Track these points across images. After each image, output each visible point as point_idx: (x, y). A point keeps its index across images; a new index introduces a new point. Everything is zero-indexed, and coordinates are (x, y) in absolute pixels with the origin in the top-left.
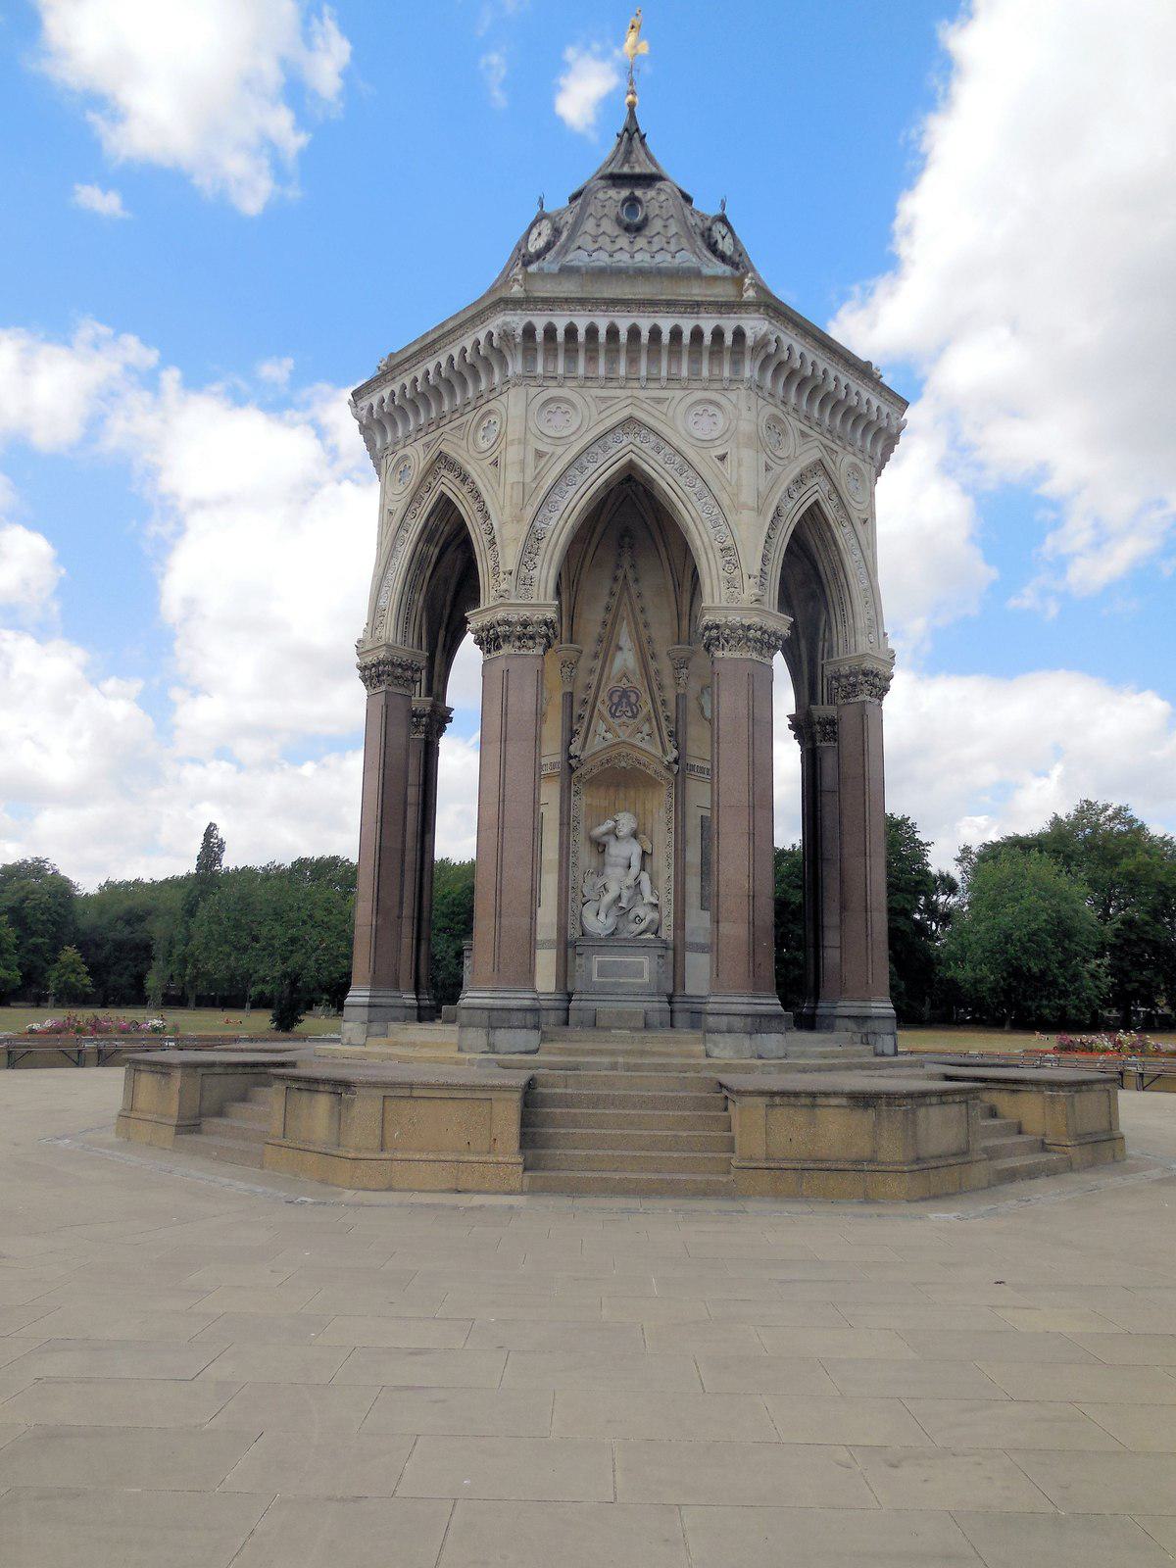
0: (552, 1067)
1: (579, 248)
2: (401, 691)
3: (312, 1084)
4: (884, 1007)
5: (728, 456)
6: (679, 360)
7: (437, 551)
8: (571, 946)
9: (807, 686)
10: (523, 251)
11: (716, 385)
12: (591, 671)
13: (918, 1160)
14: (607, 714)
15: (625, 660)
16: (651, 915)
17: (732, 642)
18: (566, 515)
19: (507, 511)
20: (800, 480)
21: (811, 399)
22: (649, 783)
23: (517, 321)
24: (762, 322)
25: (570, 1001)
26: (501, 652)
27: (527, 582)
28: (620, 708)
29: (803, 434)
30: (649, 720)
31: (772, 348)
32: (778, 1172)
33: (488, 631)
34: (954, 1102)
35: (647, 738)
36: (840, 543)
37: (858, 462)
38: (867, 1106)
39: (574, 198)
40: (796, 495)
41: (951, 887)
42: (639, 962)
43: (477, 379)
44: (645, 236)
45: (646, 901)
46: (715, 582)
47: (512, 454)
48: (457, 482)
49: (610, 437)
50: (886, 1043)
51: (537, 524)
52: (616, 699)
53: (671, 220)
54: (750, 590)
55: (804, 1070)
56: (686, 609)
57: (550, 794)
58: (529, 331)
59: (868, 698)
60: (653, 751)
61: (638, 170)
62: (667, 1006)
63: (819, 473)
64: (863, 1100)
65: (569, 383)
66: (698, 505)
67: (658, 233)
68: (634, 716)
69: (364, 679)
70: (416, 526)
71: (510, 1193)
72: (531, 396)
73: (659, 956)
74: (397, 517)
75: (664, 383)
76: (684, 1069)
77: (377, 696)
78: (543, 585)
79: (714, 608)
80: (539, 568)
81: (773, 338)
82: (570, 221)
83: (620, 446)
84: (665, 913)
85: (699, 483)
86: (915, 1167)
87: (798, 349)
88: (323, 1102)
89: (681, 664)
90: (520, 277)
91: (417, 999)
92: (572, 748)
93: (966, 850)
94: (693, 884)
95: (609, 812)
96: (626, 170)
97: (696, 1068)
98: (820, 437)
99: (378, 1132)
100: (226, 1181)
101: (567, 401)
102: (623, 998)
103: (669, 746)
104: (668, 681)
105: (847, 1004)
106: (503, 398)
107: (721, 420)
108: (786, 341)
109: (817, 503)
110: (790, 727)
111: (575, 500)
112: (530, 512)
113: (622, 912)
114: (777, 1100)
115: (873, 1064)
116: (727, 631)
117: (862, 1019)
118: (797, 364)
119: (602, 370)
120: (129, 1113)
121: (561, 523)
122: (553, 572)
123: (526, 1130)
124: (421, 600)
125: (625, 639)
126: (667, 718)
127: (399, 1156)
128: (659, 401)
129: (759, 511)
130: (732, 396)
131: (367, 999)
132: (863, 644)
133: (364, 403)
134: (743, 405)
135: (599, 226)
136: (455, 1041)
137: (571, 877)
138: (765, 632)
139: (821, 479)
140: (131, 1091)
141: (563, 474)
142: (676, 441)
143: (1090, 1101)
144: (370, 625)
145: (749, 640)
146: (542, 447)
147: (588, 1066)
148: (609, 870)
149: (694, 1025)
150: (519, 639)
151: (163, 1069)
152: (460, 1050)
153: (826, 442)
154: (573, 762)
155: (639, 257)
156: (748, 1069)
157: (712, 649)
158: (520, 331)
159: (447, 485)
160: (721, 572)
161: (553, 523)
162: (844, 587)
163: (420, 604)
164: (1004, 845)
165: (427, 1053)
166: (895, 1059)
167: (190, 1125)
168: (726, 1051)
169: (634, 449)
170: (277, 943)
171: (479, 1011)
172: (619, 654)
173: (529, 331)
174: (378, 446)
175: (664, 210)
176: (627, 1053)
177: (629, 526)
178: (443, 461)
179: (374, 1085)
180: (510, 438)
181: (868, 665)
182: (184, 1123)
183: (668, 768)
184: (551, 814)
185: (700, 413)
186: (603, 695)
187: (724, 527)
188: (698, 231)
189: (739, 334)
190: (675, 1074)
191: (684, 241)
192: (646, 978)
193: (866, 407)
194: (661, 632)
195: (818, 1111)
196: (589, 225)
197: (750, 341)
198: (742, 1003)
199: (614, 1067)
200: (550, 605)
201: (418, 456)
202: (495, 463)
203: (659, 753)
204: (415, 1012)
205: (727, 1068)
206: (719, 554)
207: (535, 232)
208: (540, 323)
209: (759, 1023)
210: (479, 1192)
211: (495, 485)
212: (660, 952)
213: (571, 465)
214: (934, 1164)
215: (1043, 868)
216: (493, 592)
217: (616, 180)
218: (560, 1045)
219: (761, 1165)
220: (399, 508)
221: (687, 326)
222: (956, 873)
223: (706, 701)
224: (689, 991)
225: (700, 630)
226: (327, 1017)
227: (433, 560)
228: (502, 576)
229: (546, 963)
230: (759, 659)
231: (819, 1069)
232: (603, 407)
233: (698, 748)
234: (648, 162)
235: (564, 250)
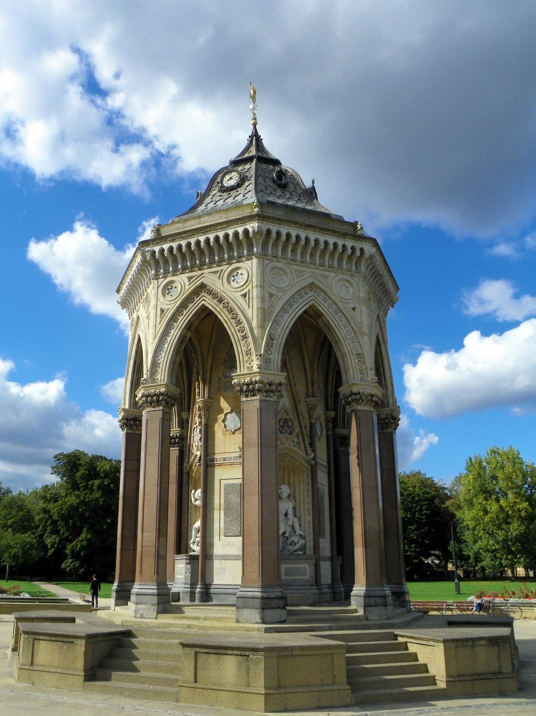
5: (357, 308)
18: (285, 328)
35: (296, 445)
46: (355, 370)
49: (303, 291)
52: (282, 424)
68: (291, 433)
70: (182, 321)
72: (265, 265)
78: (275, 363)
80: (273, 354)
83: (308, 296)
85: (344, 319)
101: (283, 270)
102: (299, 588)
103: (309, 450)
111: (289, 320)
114: (459, 644)
121: (283, 332)
123: (350, 667)
130: (356, 279)
136: (234, 616)
141: (282, 308)
142: (334, 298)
146: (273, 292)
150: (266, 392)
152: (238, 621)
160: (357, 366)
161: (279, 331)
171: (252, 600)
182: (452, 679)
187: (356, 343)
192: (308, 577)
206: (355, 357)
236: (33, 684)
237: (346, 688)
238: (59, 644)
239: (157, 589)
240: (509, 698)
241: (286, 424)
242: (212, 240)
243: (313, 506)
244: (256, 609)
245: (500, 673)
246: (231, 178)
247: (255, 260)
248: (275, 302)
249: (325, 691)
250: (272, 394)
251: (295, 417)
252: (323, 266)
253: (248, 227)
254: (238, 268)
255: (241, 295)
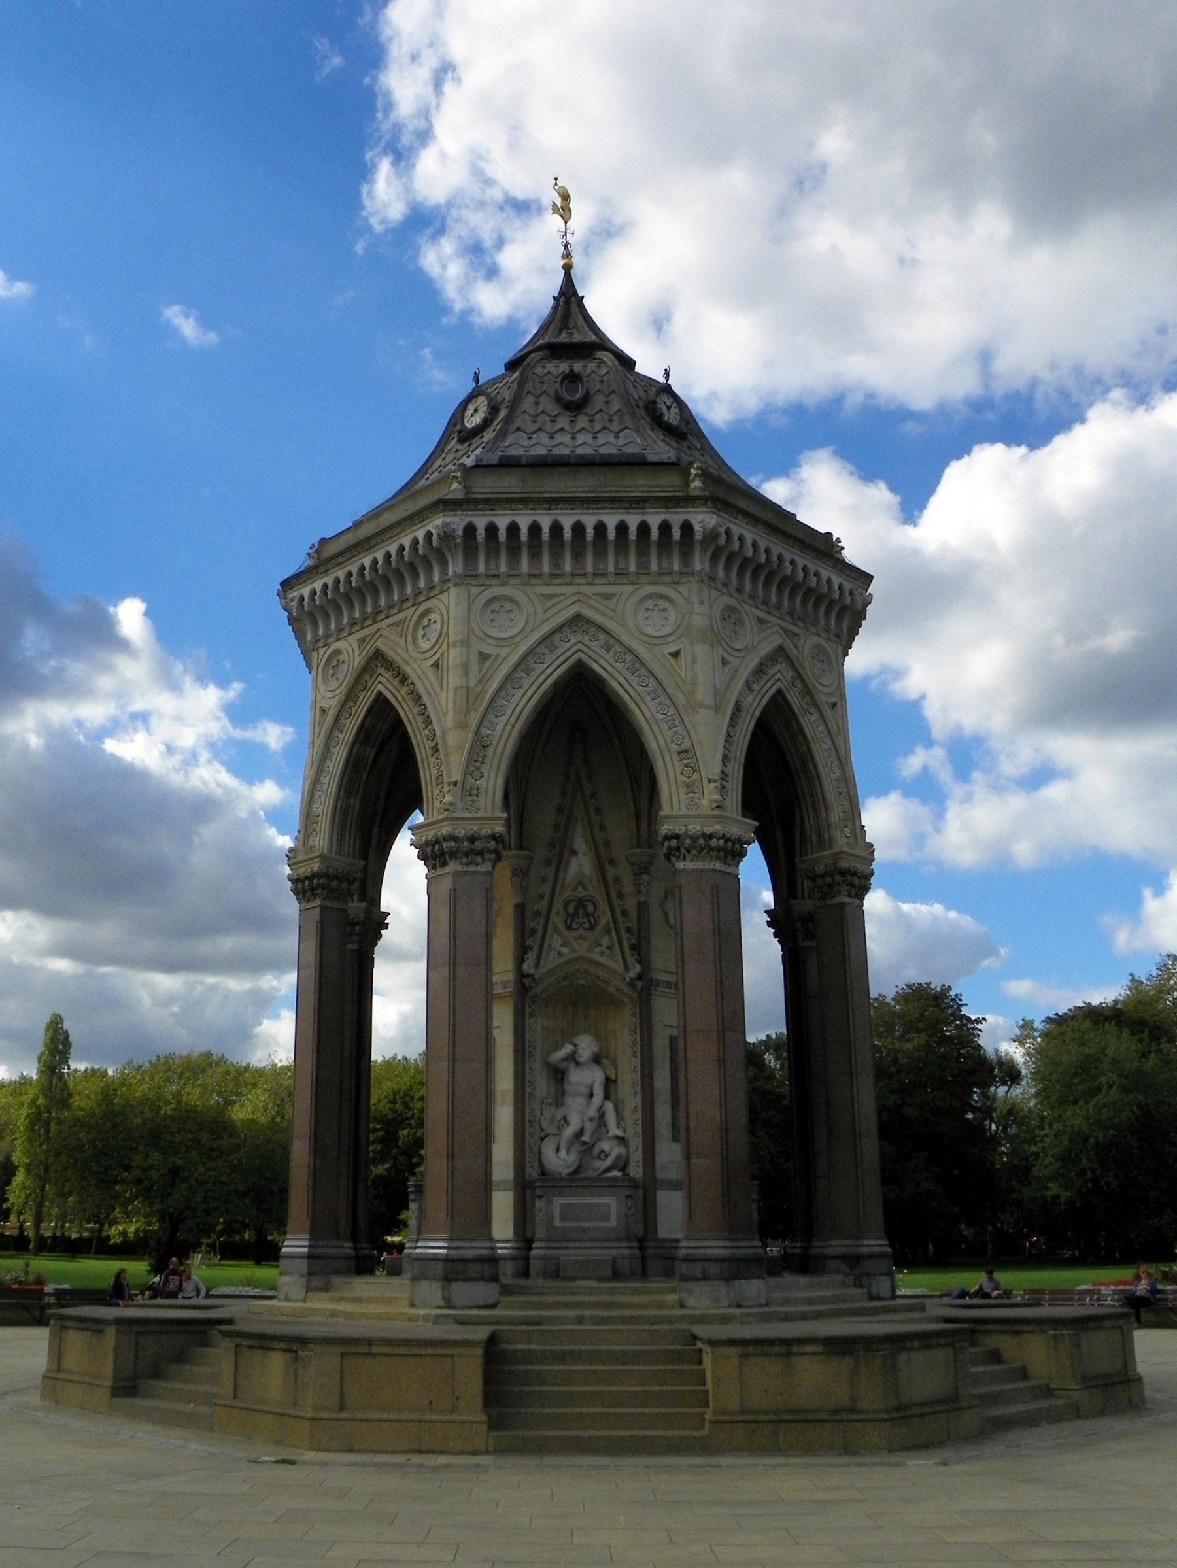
0: (512, 1321)
1: (518, 429)
2: (335, 904)
3: (263, 1341)
4: (876, 1244)
6: (627, 553)
7: (374, 751)
8: (530, 1186)
9: (784, 878)
10: (459, 427)
11: (667, 579)
12: (544, 880)
13: (898, 1408)
14: (561, 926)
15: (580, 865)
16: (617, 1150)
17: (694, 852)
18: (513, 720)
19: (450, 717)
20: (760, 671)
21: (767, 583)
22: (610, 1002)
23: (457, 522)
24: (710, 515)
25: (530, 1248)
26: (447, 869)
27: (471, 793)
29: (761, 621)
30: (608, 931)
31: (722, 540)
32: (754, 1426)
33: (433, 846)
34: (938, 1346)
35: (608, 952)
36: (807, 732)
37: (823, 643)
38: (843, 1354)
39: (511, 366)
40: (756, 687)
41: (1011, 1074)
42: (604, 1204)
43: (415, 575)
44: (587, 414)
45: (611, 1134)
46: (674, 788)
47: (454, 657)
48: (396, 682)
50: (882, 1286)
51: (483, 730)
52: (571, 909)
53: (613, 396)
54: (709, 795)
55: (787, 1318)
56: (644, 808)
57: (503, 1018)
58: (470, 530)
59: (847, 900)
60: (611, 964)
61: (577, 338)
62: (637, 1252)
63: (781, 659)
64: (838, 1346)
65: (513, 581)
66: (652, 705)
67: (600, 410)
68: (592, 928)
69: (296, 892)
70: (351, 727)
71: (474, 1453)
72: (472, 597)
73: (627, 1197)
74: (331, 715)
75: (612, 579)
76: (655, 1321)
77: (311, 911)
79: (672, 817)
81: (722, 530)
82: (508, 398)
83: (568, 645)
84: (632, 1148)
86: (896, 1415)
87: (749, 537)
88: (276, 1361)
89: (642, 870)
90: (459, 474)
91: (355, 1248)
92: (525, 966)
93: (1027, 1025)
94: (663, 1113)
95: (568, 1035)
96: (564, 338)
97: (669, 1320)
98: (780, 622)
99: (337, 1390)
100: (180, 1443)
101: (511, 599)
102: (588, 1244)
103: (631, 960)
104: (628, 888)
105: (835, 1242)
106: (444, 597)
107: (672, 615)
108: (736, 530)
109: (779, 691)
110: (769, 924)
111: (523, 702)
112: (475, 718)
113: (586, 1147)
114: (751, 1349)
115: (865, 1309)
116: (688, 841)
117: (853, 1260)
118: (750, 554)
119: (546, 568)
120: (55, 1380)
121: (509, 728)
122: (501, 781)
124: (357, 803)
125: (580, 843)
126: (628, 930)
127: (359, 1415)
128: (608, 597)
129: (717, 708)
130: (683, 589)
131: (306, 1250)
132: (841, 841)
133: (294, 594)
134: (695, 598)
135: (537, 404)
137: (527, 1110)
138: (727, 840)
139: (782, 666)
140: (57, 1352)
141: (508, 678)
142: (625, 639)
143: (1098, 1343)
144: (302, 832)
145: (711, 849)
147: (550, 1320)
148: (569, 1100)
149: (668, 1273)
150: (467, 854)
151: (94, 1326)
152: (412, 1305)
153: (784, 625)
154: (526, 981)
155: (581, 438)
156: (725, 1320)
157: (674, 859)
158: (460, 532)
159: (384, 684)
160: (678, 775)
161: (499, 728)
162: (813, 777)
163: (356, 809)
164: (1073, 1018)
165: (373, 1309)
166: (892, 1303)
167: (127, 1386)
168: (703, 1299)
169: (583, 648)
170: (155, 1175)
171: (432, 1263)
172: (574, 860)
174: (309, 637)
175: (605, 384)
176: (597, 1305)
177: (580, 735)
178: (378, 660)
179: (327, 1341)
180: (451, 640)
181: (844, 864)
183: (631, 984)
184: (504, 1039)
186: (557, 906)
188: (641, 403)
189: (687, 527)
190: (647, 1327)
191: (627, 417)
192: (613, 1223)
193: (826, 587)
194: (619, 832)
195: (793, 1360)
196: (528, 404)
197: (698, 536)
198: (716, 1247)
199: (580, 1320)
200: (500, 818)
201: (351, 650)
202: (436, 665)
203: (618, 966)
204: (353, 1264)
205: (703, 1319)
206: (676, 757)
207: (471, 408)
208: (480, 522)
209: (736, 1269)
210: (442, 1452)
211: (438, 689)
212: (627, 1192)
213: (517, 666)
214: (916, 1411)
215: (1121, 1046)
216: (437, 804)
217: (555, 351)
218: (522, 1299)
219: (736, 1418)
220: (333, 704)
221: (633, 521)
222: (1016, 1053)
223: (670, 907)
224: (663, 1233)
225: (660, 839)
226: (208, 1265)
227: (370, 761)
228: (446, 788)
229: (503, 1204)
230: (723, 868)
231: (804, 1317)
232: (549, 604)
233: (663, 962)
234: (587, 329)
235: (502, 434)
236: (57, 1402)
237: (477, 1419)
238: (89, 1334)
241: (581, 911)
243: (642, 1076)
244: (436, 1280)
245: (851, 1410)
246: (476, 410)
247: (453, 591)
248: (491, 671)
249: (431, 1421)
250: (479, 859)
252: (604, 575)
253: (430, 527)
254: (427, 612)
255: (480, 652)
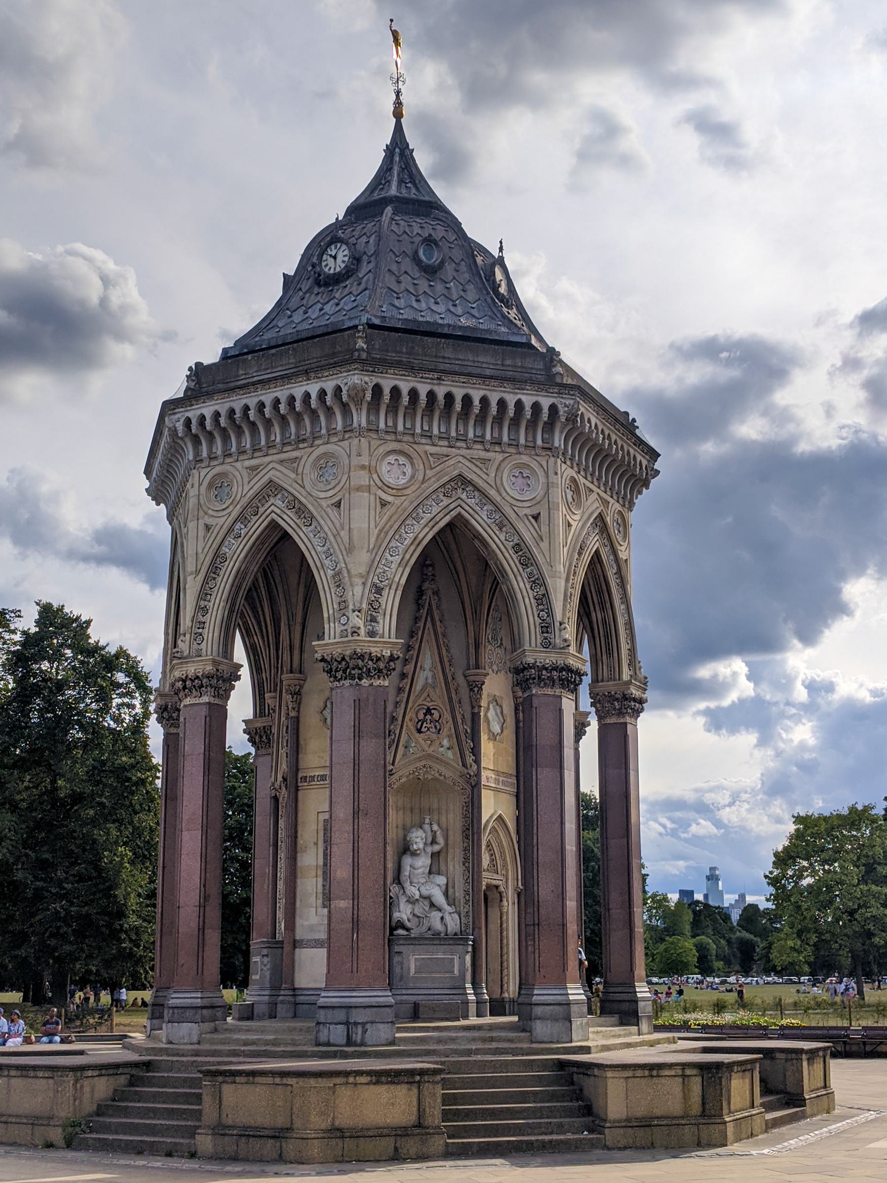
28: (425, 725)
52: (421, 716)
159: (277, 510)
173: (377, 390)
185: (525, 475)
239: (636, 992)
240: (580, 1164)
242: (314, 396)
251: (444, 704)
